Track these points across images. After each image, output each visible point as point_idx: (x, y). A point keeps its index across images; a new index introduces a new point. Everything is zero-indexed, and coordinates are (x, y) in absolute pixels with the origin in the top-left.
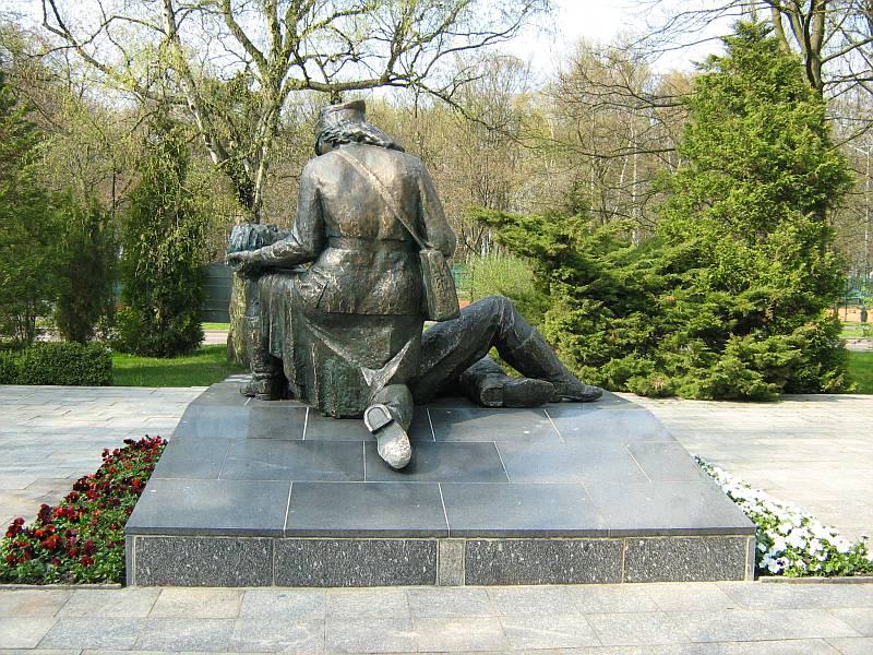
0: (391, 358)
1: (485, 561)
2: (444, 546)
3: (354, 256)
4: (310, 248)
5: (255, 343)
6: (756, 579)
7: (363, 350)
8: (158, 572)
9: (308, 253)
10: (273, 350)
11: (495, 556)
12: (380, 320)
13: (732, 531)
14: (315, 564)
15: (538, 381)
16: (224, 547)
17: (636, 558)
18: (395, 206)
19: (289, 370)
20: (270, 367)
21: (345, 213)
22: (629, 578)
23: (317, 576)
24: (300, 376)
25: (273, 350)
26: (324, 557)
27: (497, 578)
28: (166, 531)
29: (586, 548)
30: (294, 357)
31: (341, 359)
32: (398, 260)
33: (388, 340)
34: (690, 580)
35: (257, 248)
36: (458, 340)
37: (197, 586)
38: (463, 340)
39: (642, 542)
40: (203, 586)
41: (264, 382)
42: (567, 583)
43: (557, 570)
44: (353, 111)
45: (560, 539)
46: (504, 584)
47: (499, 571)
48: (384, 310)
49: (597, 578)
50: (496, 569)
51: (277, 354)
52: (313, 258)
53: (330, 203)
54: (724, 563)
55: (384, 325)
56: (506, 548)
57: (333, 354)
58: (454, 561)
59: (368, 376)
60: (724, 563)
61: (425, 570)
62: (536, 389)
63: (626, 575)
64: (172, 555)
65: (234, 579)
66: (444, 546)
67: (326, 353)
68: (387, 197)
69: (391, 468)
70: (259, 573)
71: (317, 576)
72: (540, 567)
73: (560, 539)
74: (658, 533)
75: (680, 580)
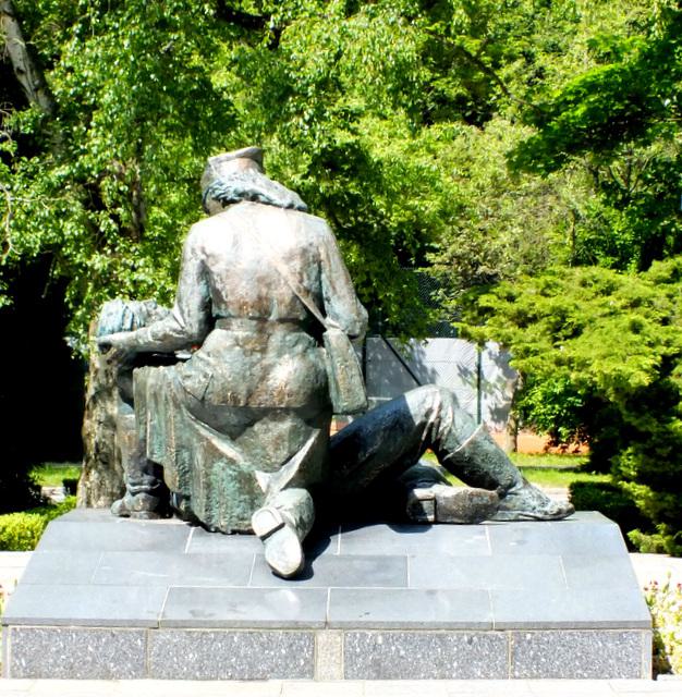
0: (290, 458)
1: (364, 653)
2: (322, 637)
3: (247, 340)
4: (194, 329)
5: (130, 448)
6: (654, 678)
7: (258, 451)
8: (33, 664)
9: (191, 336)
10: (152, 453)
11: (374, 649)
12: (273, 413)
13: (624, 625)
14: (191, 656)
15: (478, 490)
16: (99, 638)
17: (523, 653)
18: (293, 282)
19: (171, 477)
20: (147, 478)
21: (239, 290)
22: (517, 674)
23: (193, 668)
24: (167, 403)
25: (152, 453)
26: (199, 649)
27: (378, 672)
28: (41, 622)
29: (470, 642)
30: (176, 460)
31: (232, 462)
32: (296, 343)
33: (286, 438)
34: (582, 677)
35: (132, 329)
36: (379, 442)
37: (72, 678)
38: (385, 441)
39: (529, 636)
40: (78, 678)
41: (141, 496)
42: (450, 677)
43: (441, 665)
44: (246, 160)
45: (443, 631)
46: (385, 678)
47: (379, 665)
48: (281, 402)
49: (482, 673)
50: (377, 663)
51: (156, 459)
52: (196, 343)
53: (216, 278)
54: (618, 659)
55: (282, 420)
56: (386, 640)
57: (221, 456)
58: (332, 654)
59: (262, 479)
60: (618, 659)
61: (302, 663)
62: (475, 499)
63: (513, 671)
64: (46, 646)
65: (109, 671)
66: (322, 637)
67: (213, 454)
68: (284, 269)
69: (277, 574)
70: (134, 666)
71: (193, 668)
72: (422, 661)
73: (443, 631)
74: (546, 626)
75: (571, 677)
